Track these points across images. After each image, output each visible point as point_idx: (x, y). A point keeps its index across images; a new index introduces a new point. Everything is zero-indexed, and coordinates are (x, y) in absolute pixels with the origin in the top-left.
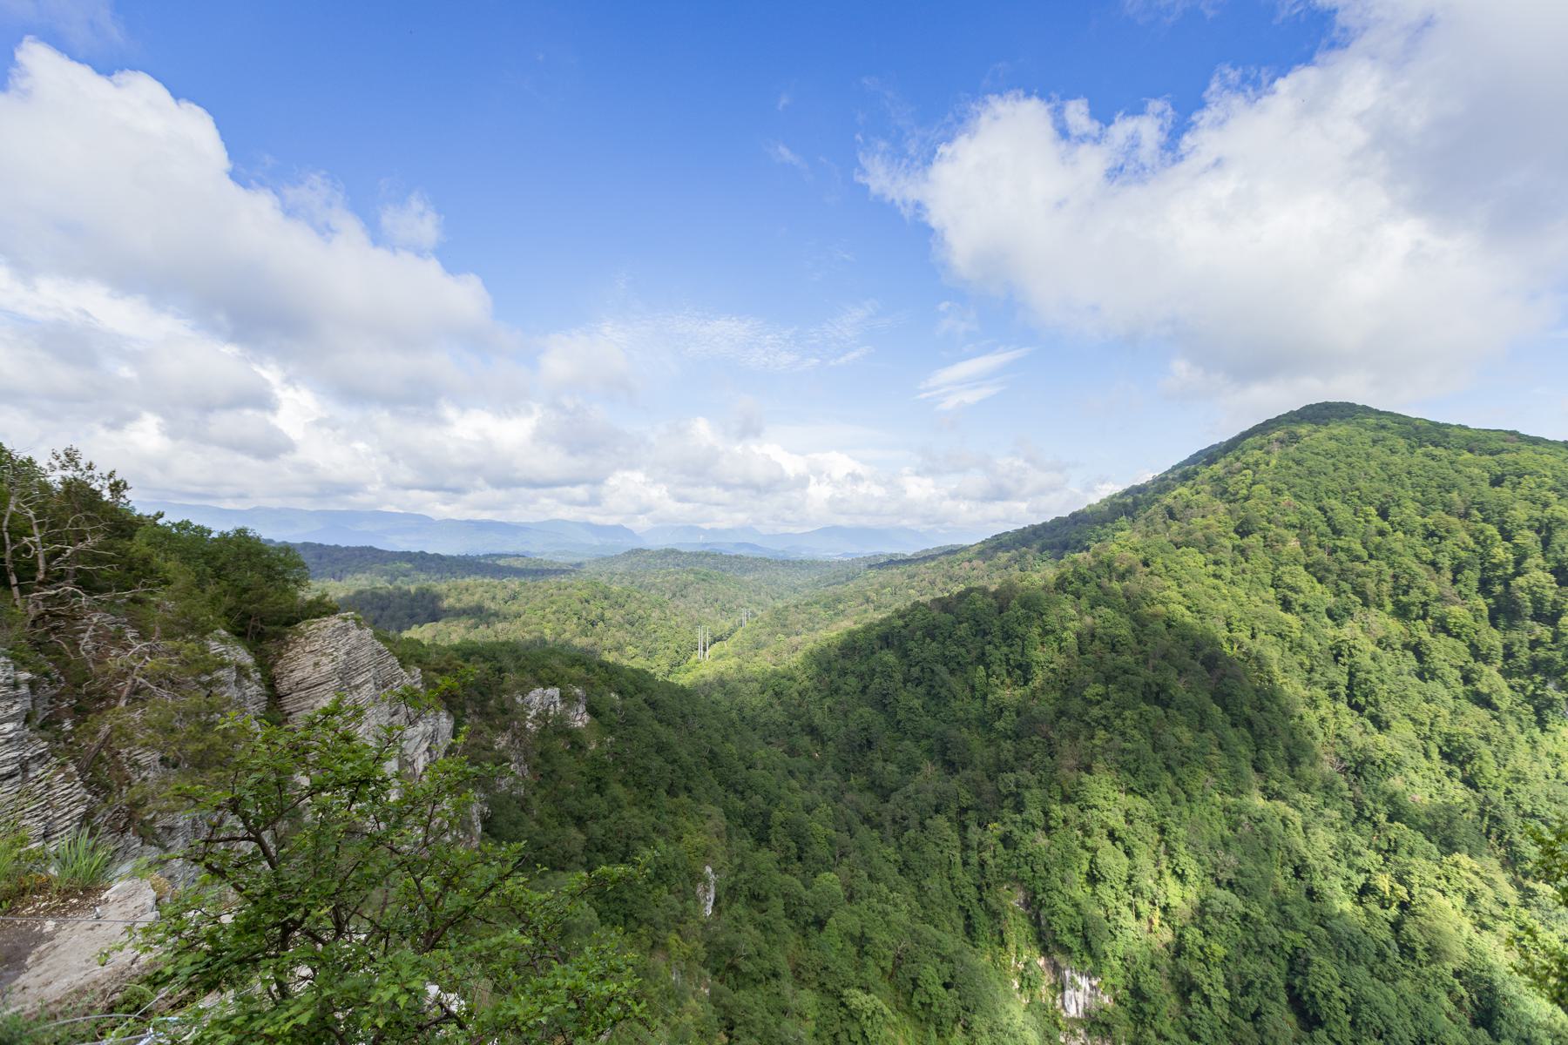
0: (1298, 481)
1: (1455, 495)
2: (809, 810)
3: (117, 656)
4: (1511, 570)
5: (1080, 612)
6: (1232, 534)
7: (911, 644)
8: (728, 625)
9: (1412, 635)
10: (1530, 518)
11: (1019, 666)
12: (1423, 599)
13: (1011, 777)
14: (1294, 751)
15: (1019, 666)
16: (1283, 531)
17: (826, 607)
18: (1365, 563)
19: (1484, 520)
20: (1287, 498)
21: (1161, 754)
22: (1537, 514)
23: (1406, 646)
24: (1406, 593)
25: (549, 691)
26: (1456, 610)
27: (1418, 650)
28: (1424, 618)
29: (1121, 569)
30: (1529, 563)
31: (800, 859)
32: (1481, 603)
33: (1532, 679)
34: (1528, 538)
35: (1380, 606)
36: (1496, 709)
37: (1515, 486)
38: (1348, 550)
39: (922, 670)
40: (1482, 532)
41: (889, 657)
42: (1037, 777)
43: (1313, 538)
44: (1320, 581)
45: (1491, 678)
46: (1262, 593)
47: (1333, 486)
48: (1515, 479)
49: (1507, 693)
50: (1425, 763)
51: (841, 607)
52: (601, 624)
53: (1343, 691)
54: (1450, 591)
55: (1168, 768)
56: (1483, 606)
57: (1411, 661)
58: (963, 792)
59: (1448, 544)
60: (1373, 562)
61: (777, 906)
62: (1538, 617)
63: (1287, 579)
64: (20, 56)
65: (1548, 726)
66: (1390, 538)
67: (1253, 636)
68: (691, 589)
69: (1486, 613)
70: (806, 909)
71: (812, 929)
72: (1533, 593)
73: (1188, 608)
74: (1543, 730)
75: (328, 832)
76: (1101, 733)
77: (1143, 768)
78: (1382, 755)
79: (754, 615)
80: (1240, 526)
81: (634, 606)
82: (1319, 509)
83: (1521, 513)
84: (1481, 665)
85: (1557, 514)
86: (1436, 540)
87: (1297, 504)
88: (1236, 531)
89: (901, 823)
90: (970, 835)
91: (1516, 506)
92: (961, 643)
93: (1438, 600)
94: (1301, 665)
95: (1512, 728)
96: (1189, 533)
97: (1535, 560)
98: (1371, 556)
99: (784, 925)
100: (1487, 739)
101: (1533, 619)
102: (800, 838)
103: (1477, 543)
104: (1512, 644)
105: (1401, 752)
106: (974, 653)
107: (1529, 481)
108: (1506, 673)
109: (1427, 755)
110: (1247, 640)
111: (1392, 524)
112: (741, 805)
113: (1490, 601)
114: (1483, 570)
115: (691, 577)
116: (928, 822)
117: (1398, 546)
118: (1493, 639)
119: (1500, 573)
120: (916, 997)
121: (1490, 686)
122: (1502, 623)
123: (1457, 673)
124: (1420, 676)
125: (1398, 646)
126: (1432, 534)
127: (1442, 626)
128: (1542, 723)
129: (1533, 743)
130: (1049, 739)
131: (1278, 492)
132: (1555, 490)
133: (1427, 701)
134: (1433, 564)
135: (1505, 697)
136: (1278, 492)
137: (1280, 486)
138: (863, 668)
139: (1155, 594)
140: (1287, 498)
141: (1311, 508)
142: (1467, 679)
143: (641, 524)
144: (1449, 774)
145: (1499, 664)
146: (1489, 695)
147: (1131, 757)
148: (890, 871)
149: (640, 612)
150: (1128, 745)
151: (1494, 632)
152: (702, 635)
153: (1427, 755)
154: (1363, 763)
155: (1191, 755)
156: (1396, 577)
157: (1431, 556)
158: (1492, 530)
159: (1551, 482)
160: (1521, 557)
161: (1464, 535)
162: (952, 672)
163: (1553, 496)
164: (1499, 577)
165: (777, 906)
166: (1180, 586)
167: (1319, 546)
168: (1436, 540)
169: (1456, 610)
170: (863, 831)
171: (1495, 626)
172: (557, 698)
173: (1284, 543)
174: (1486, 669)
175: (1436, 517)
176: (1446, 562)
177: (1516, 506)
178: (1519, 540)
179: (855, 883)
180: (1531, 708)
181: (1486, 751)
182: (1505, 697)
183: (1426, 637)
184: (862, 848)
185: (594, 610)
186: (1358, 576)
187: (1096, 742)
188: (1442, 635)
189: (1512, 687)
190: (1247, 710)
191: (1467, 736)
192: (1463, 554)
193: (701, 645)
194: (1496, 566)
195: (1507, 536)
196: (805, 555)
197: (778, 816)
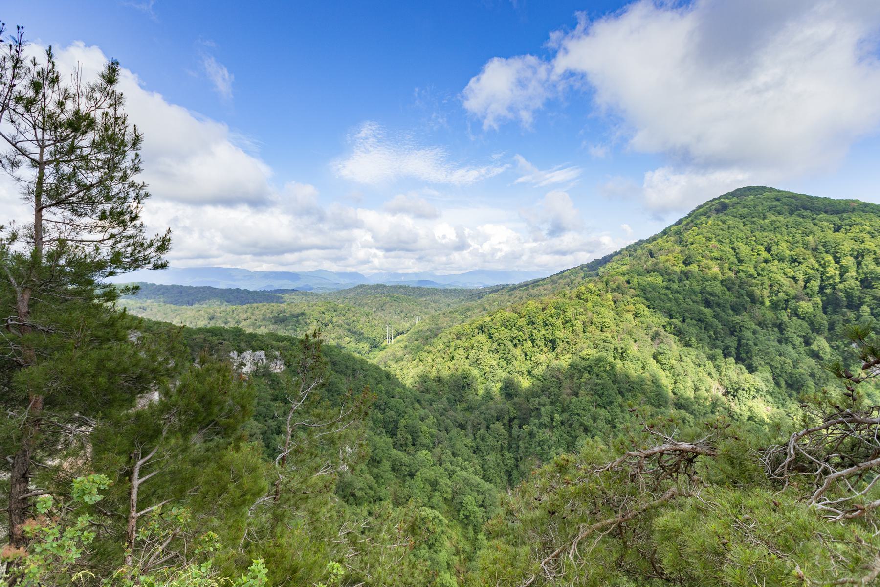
0: (721, 232)
1: (811, 238)
2: (422, 419)
4: (837, 280)
5: (586, 310)
6: (681, 265)
7: (493, 331)
8: (407, 325)
9: (778, 319)
10: (852, 250)
11: (551, 341)
12: (786, 298)
13: (537, 400)
14: (697, 384)
15: (551, 341)
16: (710, 262)
17: (461, 313)
19: (826, 252)
20: (714, 242)
21: (617, 385)
22: (856, 247)
23: (774, 325)
24: (776, 295)
25: (258, 353)
27: (780, 327)
28: (785, 309)
29: (614, 286)
31: (413, 444)
34: (848, 261)
36: (822, 359)
37: (847, 231)
38: (745, 272)
39: (499, 345)
41: (482, 338)
42: (550, 399)
44: (729, 289)
46: (694, 297)
47: (741, 235)
48: (848, 228)
51: (469, 313)
52: (330, 325)
55: (620, 393)
56: (819, 301)
57: (775, 334)
58: (512, 409)
59: (803, 267)
60: (759, 278)
61: (386, 465)
62: (850, 306)
63: (709, 288)
67: (684, 321)
68: (387, 306)
69: (820, 305)
70: (404, 468)
71: (408, 478)
75: (217, 453)
76: (586, 375)
77: (606, 393)
78: (748, 385)
79: (422, 319)
80: (686, 260)
81: (351, 315)
82: (732, 248)
83: (847, 246)
84: (815, 334)
85: (868, 247)
87: (719, 246)
88: (684, 263)
89: (476, 427)
90: (514, 432)
91: (845, 243)
92: (520, 329)
93: (794, 298)
94: (710, 337)
97: (852, 273)
98: (759, 275)
99: (390, 475)
100: (812, 375)
102: (414, 435)
106: (527, 335)
107: (856, 229)
108: (829, 340)
111: (772, 255)
112: (381, 417)
113: (825, 298)
114: (822, 281)
115: (388, 299)
116: (492, 425)
117: (774, 268)
119: (831, 281)
120: (461, 512)
121: (819, 346)
122: (829, 310)
123: (800, 340)
124: (780, 342)
126: (795, 261)
130: (559, 379)
131: (709, 239)
132: (869, 233)
133: (780, 355)
134: (794, 278)
136: (709, 239)
137: (710, 235)
138: (467, 345)
140: (714, 242)
141: (727, 249)
142: (807, 343)
143: (364, 270)
144: (790, 396)
147: (599, 388)
148: (468, 452)
149: (354, 318)
150: (599, 381)
151: (824, 316)
152: (390, 331)
154: (738, 389)
155: (634, 386)
156: (771, 286)
157: (793, 273)
158: (829, 258)
159: (868, 229)
160: (844, 271)
161: (812, 261)
162: (515, 346)
163: (867, 237)
164: (830, 284)
165: (386, 465)
167: (730, 269)
168: (797, 264)
169: (803, 304)
170: (454, 431)
171: (825, 313)
172: (263, 356)
173: (709, 268)
174: (818, 337)
175: (799, 250)
176: (801, 277)
177: (845, 243)
178: (843, 262)
179: (443, 457)
181: (811, 382)
184: (450, 439)
185: (327, 317)
186: (750, 286)
187: (583, 380)
189: (832, 347)
190: (673, 362)
192: (811, 272)
193: (388, 336)
195: (837, 260)
196: (459, 286)
197: (402, 422)
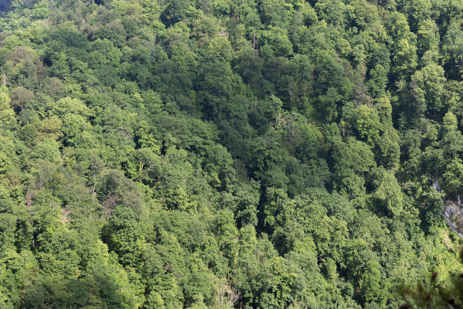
3: (257, 286)
4: (414, 64)
9: (326, 140)
12: (339, 98)
16: (212, 20)
18: (290, 57)
24: (324, 92)
26: (366, 109)
28: (337, 121)
30: (429, 54)
32: (386, 100)
33: (420, 180)
34: (429, 28)
35: (301, 109)
36: (391, 216)
38: (275, 42)
40: (394, 21)
43: (241, 27)
45: (389, 185)
46: (181, 97)
49: (400, 197)
50: (325, 284)
53: (253, 211)
54: (362, 90)
60: (297, 57)
64: (453, 287)
65: (431, 229)
66: (314, 28)
67: (163, 151)
72: (427, 87)
73: (91, 119)
74: (427, 233)
80: (167, 12)
86: (355, 29)
95: (400, 235)
96: (107, 20)
97: (433, 52)
98: (296, 49)
100: (377, 248)
101: (427, 116)
103: (390, 34)
104: (409, 145)
105: (298, 275)
109: (325, 272)
110: (155, 157)
113: (396, 98)
114: (393, 64)
117: (320, 37)
118: (392, 139)
122: (402, 121)
125: (314, 154)
127: (354, 131)
128: (425, 226)
129: (417, 248)
135: (400, 204)
139: (50, 102)
145: (397, 166)
146: (386, 201)
153: (325, 272)
158: (402, 19)
164: (404, 71)
166: (84, 90)
167: (247, 37)
168: (355, 29)
173: (211, 34)
176: (362, 56)
180: (417, 212)
181: (374, 261)
182: (400, 204)
183: (338, 140)
188: (352, 139)
189: (405, 191)
190: (142, 244)
191: (360, 248)
192: (377, 46)
194: (404, 59)
